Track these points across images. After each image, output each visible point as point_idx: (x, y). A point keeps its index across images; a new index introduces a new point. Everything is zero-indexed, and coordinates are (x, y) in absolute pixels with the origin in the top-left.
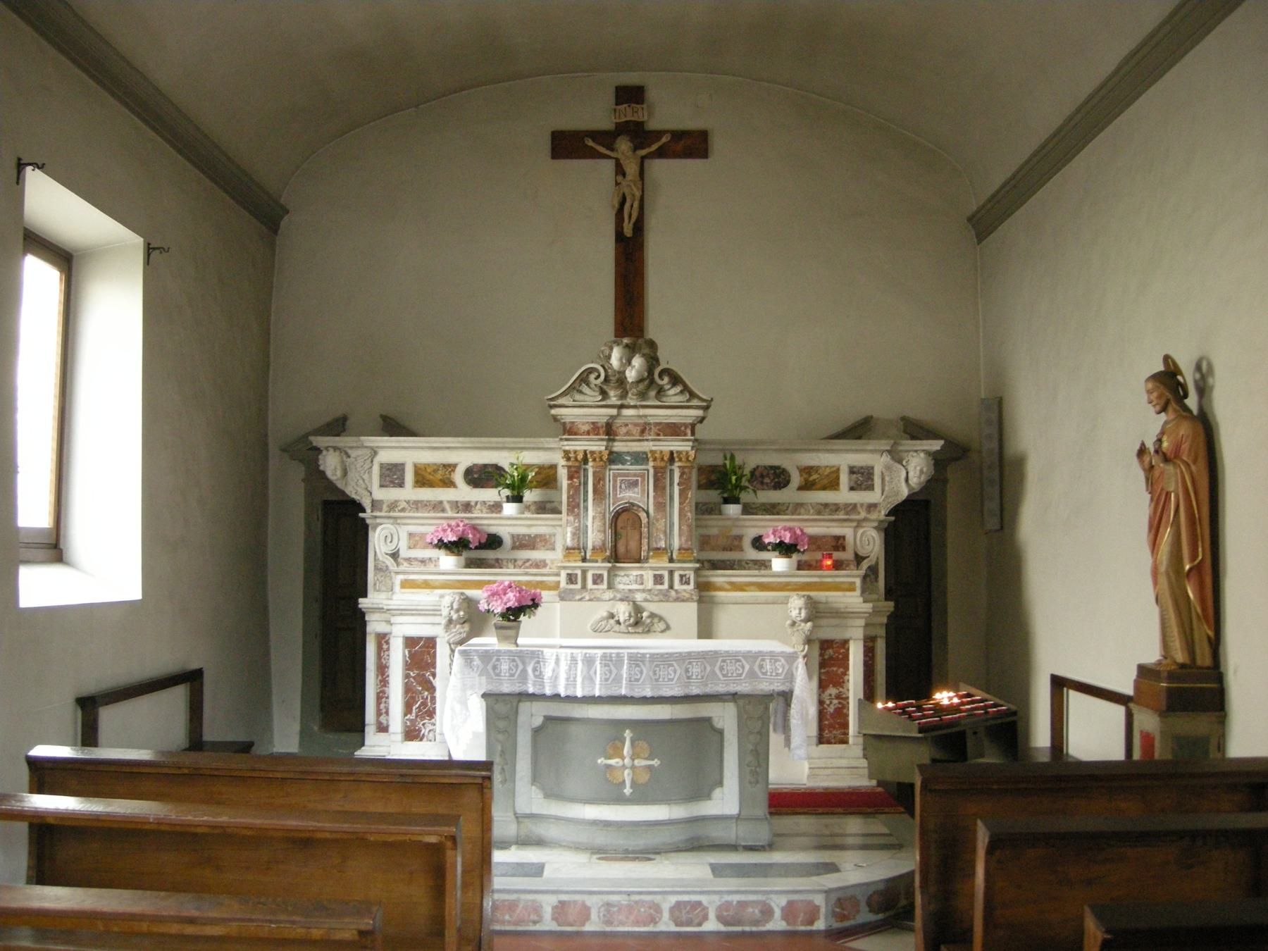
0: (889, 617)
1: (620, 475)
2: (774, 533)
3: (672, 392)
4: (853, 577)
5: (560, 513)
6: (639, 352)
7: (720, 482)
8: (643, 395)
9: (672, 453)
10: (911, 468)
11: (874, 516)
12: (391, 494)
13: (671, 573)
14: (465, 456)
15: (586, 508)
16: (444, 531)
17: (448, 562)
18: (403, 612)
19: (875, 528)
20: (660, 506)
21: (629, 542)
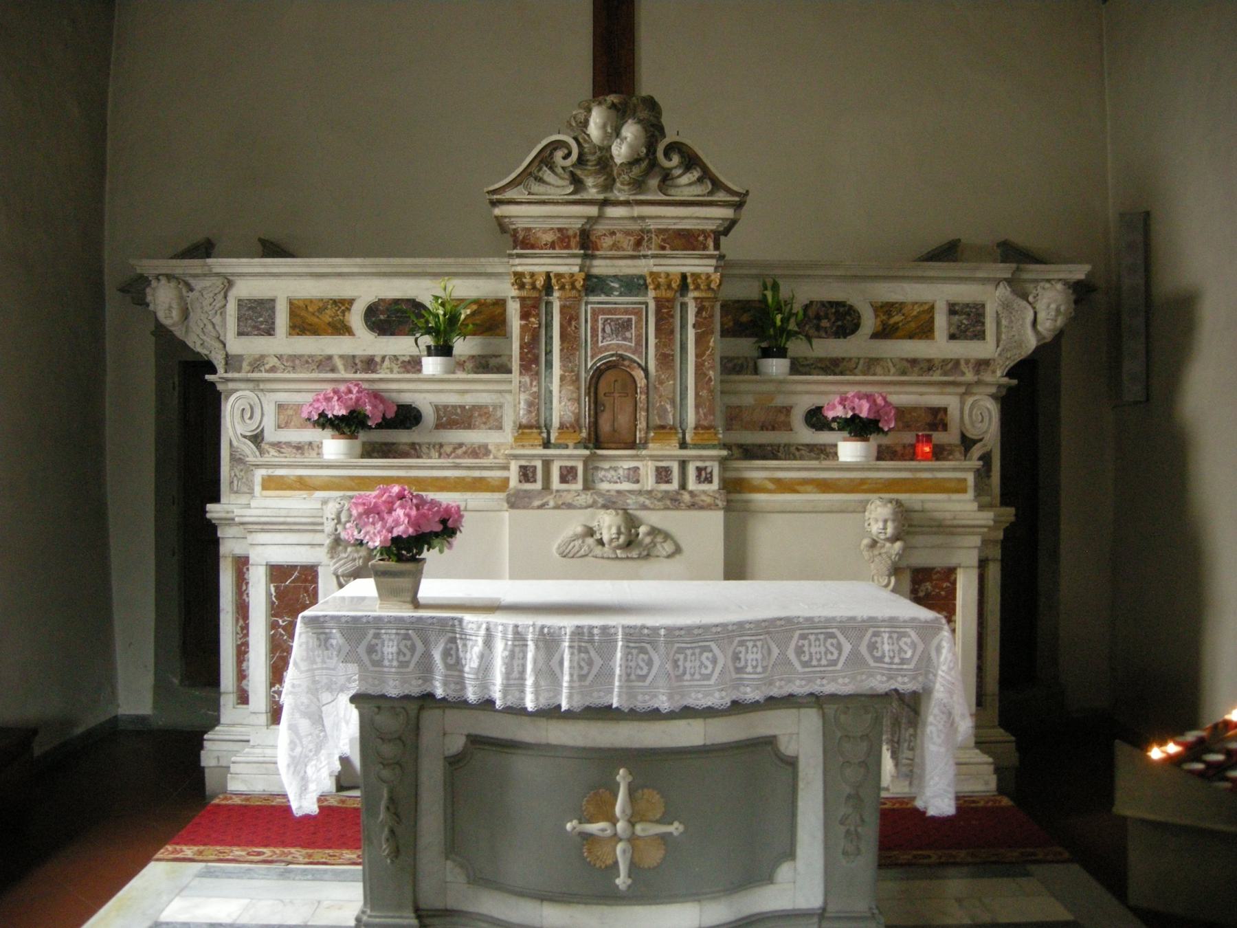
0: (1005, 530)
1: (603, 311)
2: (843, 401)
3: (685, 180)
4: (963, 470)
5: (509, 372)
6: (633, 114)
7: (756, 325)
8: (638, 185)
9: (684, 277)
10: (1041, 306)
11: (987, 377)
12: (256, 345)
13: (683, 464)
14: (367, 287)
15: (549, 365)
16: (328, 400)
17: (333, 447)
18: (266, 526)
19: (993, 396)
20: (665, 360)
21: (616, 418)
